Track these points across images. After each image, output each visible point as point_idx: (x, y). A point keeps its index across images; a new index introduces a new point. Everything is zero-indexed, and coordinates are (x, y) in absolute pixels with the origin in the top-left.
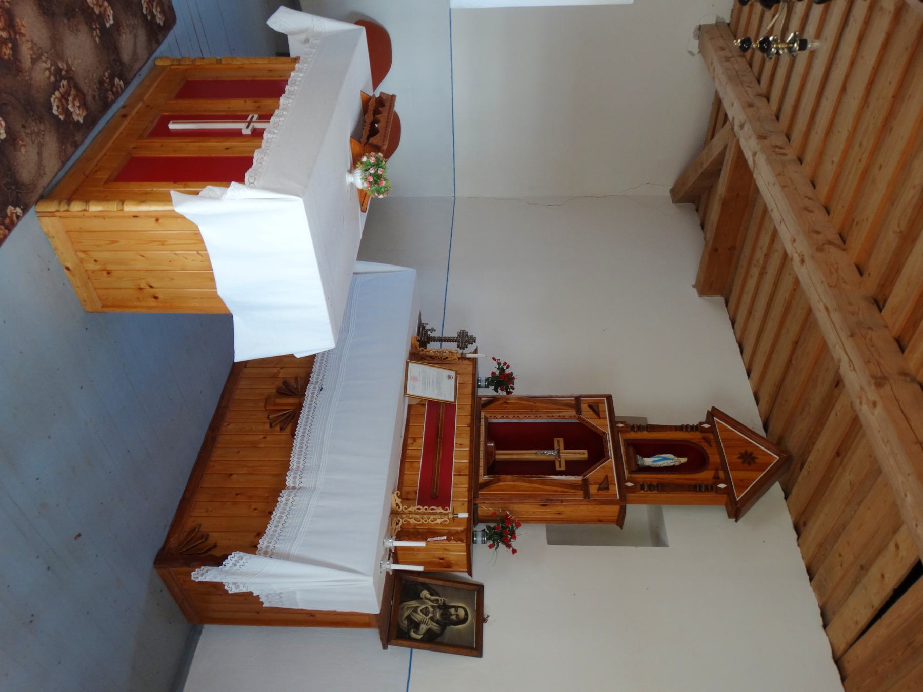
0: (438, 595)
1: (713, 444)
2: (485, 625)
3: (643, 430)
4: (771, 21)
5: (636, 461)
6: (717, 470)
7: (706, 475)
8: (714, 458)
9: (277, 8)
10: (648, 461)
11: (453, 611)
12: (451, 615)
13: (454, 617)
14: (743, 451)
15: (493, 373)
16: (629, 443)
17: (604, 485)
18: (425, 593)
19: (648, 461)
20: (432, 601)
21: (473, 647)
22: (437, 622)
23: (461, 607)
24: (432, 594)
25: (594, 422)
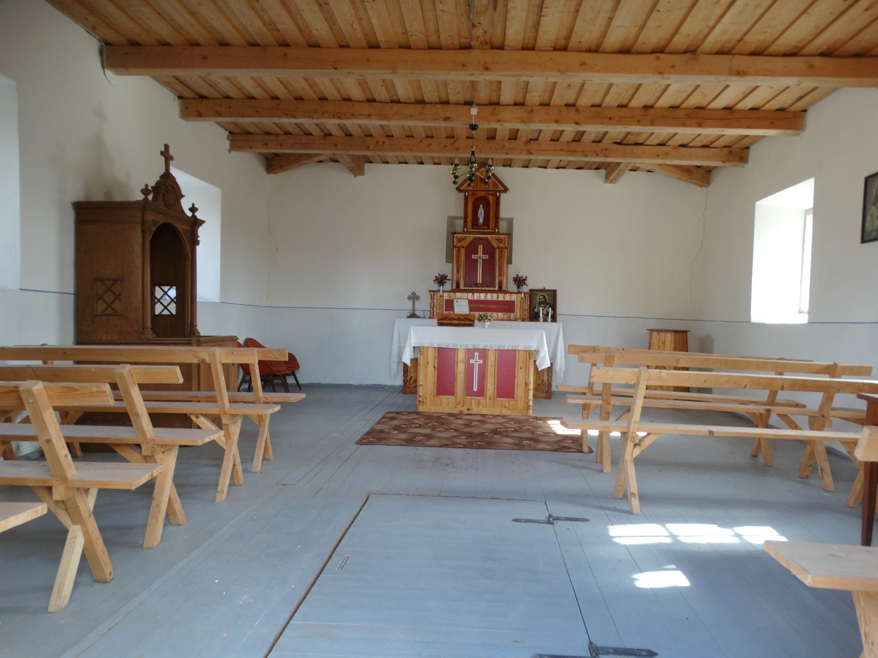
0: (536, 306)
1: (475, 192)
2: (546, 288)
3: (467, 221)
4: (763, 137)
5: (481, 225)
6: (488, 194)
7: (491, 199)
8: (483, 194)
9: (753, 323)
10: (481, 221)
11: (541, 300)
13: (543, 300)
14: (479, 181)
15: (522, 277)
18: (536, 310)
19: (481, 221)
21: (554, 292)
22: (546, 306)
23: (539, 297)
25: (468, 241)
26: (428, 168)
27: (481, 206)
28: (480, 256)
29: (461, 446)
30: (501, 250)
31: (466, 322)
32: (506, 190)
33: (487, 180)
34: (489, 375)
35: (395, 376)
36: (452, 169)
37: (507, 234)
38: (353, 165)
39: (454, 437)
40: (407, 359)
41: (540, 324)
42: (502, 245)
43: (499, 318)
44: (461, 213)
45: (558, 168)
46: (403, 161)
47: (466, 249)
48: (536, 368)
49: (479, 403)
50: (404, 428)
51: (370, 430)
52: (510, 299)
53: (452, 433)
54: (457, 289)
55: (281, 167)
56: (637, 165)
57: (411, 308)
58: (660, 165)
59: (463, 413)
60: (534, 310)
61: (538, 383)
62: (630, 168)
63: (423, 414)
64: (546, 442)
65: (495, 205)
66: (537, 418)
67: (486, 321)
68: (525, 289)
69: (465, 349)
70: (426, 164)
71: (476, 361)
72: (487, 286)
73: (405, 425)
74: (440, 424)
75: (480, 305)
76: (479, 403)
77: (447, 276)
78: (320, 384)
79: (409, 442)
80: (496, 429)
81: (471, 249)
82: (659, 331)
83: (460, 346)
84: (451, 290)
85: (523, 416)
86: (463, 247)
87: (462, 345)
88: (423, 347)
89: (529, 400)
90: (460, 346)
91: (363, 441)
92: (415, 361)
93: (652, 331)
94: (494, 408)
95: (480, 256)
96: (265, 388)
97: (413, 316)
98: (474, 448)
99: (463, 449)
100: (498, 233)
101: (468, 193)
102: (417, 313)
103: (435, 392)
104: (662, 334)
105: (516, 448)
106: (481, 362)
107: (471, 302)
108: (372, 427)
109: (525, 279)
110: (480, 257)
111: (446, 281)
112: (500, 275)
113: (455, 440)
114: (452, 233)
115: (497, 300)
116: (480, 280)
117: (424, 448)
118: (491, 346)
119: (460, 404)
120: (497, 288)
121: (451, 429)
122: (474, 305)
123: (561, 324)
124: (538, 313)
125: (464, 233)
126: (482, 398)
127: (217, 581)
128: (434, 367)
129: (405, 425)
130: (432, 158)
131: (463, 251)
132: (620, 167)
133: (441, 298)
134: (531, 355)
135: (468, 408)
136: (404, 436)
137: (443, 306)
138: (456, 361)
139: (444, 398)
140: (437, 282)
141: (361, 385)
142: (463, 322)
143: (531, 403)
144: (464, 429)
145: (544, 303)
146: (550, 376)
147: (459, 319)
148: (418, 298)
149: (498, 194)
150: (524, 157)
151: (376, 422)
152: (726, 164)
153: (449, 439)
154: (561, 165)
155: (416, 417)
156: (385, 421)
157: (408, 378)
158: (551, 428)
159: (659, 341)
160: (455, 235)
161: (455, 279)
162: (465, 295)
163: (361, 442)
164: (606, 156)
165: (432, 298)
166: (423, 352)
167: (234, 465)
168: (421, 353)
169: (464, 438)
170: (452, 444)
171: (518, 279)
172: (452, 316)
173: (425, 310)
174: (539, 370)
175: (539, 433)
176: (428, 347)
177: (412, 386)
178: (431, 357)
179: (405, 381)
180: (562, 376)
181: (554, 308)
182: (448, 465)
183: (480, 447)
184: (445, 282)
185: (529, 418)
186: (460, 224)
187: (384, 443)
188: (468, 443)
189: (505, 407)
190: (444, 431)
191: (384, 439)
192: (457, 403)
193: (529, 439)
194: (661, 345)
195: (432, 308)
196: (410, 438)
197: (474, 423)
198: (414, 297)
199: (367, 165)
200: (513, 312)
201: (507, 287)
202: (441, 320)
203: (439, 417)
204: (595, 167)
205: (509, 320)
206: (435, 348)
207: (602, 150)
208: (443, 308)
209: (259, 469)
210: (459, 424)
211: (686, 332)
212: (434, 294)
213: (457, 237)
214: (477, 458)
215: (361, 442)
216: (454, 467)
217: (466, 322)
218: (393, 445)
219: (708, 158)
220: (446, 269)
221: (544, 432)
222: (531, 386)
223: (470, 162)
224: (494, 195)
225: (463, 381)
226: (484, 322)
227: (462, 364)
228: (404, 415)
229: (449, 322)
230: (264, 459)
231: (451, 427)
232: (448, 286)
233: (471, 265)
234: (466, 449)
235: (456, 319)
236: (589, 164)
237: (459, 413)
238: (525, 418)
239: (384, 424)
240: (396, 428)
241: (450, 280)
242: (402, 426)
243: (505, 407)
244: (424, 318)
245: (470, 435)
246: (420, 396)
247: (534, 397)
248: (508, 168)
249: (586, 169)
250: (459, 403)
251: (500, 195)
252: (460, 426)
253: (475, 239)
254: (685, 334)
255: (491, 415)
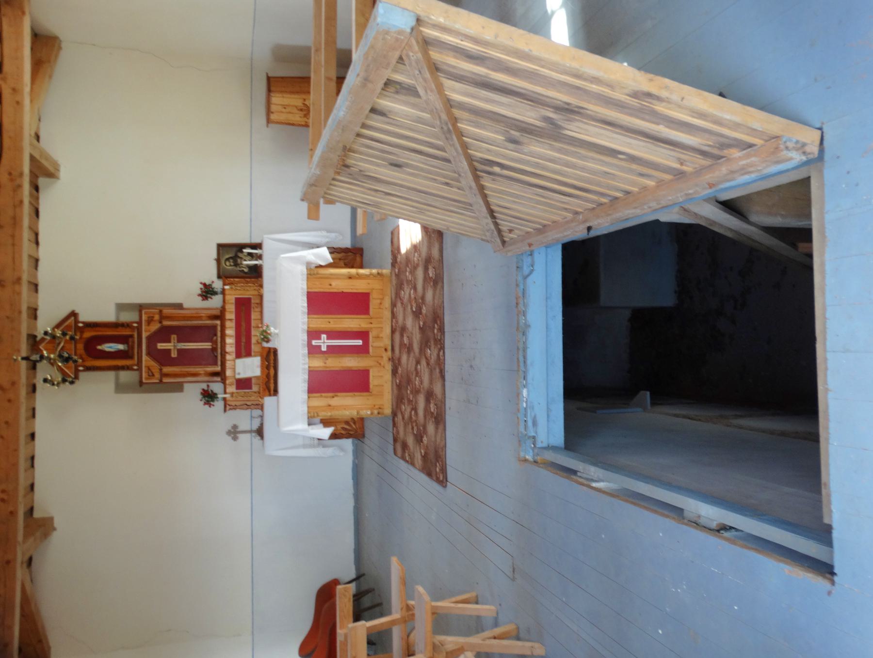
0: (239, 270)
5: (128, 347)
7: (88, 334)
8: (80, 346)
10: (121, 347)
12: (233, 262)
13: (231, 261)
15: (201, 289)
16: (131, 357)
17: (150, 321)
18: (246, 270)
19: (121, 347)
20: (243, 267)
21: (221, 247)
23: (228, 266)
24: (243, 270)
25: (152, 363)
26: (41, 425)
27: (99, 347)
28: (172, 346)
29: (441, 353)
30: (163, 318)
31: (272, 357)
32: (74, 314)
33: (68, 337)
34: (341, 326)
35: (342, 449)
36: (52, 387)
37: (140, 311)
38: (38, 534)
39: (428, 364)
40: (325, 432)
41: (266, 264)
42: (157, 317)
43: (259, 317)
44: (111, 374)
45: (37, 243)
46: (29, 462)
47: (162, 366)
48: (329, 266)
49: (377, 337)
50: (418, 429)
51: (423, 473)
52: (232, 303)
53: (423, 366)
54: (221, 375)
55: (40, 641)
56: (33, 134)
57: (248, 435)
58: (31, 101)
59: (391, 358)
60: (246, 273)
61: (343, 265)
62: (35, 142)
63: (394, 407)
64: (430, 248)
65: (97, 329)
66: (393, 265)
67: (269, 332)
68: (218, 285)
69: (309, 357)
70: (34, 428)
71: (324, 342)
72: (216, 335)
73: (413, 428)
74: (408, 384)
75: (243, 344)
76: (377, 337)
77: (203, 390)
78: (355, 549)
79: (439, 419)
80: (413, 311)
81: (163, 358)
82: (269, 112)
83: (304, 364)
84: (223, 383)
85: (391, 281)
86: (161, 370)
87: (303, 362)
88: (309, 412)
89: (371, 274)
90: (304, 364)
91: (441, 478)
92: (326, 423)
93: (269, 121)
94: (382, 318)
95: (172, 346)
96: (389, 613)
97: (260, 432)
98: (444, 337)
99: (446, 351)
100: (140, 323)
101: (80, 366)
102: (255, 426)
103: (365, 394)
104: (273, 108)
105: (440, 284)
106: (324, 336)
107: (239, 355)
108: (419, 470)
109: (205, 285)
110: (175, 346)
111: (209, 390)
112: (199, 318)
113: (432, 361)
114: (141, 386)
115: (234, 321)
116: (207, 345)
117: (447, 400)
118: (303, 323)
119: (379, 362)
120: (218, 322)
121: (416, 369)
122: (244, 350)
123: (265, 236)
124: (250, 267)
125: (140, 370)
126: (370, 333)
127: (660, 632)
128: (333, 397)
129: (413, 428)
130: (27, 419)
131: (167, 370)
132: (37, 156)
133: (234, 395)
134: (314, 272)
135: (384, 350)
136: (431, 428)
137: (244, 392)
138: (325, 369)
139: (373, 382)
140: (212, 403)
141: (354, 495)
142: (272, 362)
143: (374, 271)
144: (414, 353)
145: (235, 259)
146: (334, 250)
147: (268, 367)
148: (235, 427)
149: (81, 325)
150: (25, 289)
151: (411, 467)
152: (27, 10)
153: (431, 370)
154: (33, 238)
155: (400, 416)
156: (409, 455)
157: (343, 432)
158: (419, 242)
159: (282, 112)
160: (144, 381)
161: (206, 379)
162: (228, 364)
163: (442, 481)
164: (21, 175)
165: (235, 408)
166: (314, 413)
167: (495, 638)
168: (316, 414)
169: (429, 351)
170: (439, 365)
171: (204, 294)
172: (265, 377)
173: (251, 417)
174: (332, 261)
175: (415, 259)
176: (308, 407)
177: (354, 426)
178: (320, 401)
179: (348, 436)
180: (333, 235)
181: (240, 247)
182: (471, 366)
183: (442, 330)
184: (212, 391)
185: (393, 273)
186: (126, 376)
187: (442, 451)
188: (436, 344)
189: (381, 304)
190: (420, 377)
191: (436, 452)
192: (379, 366)
193: (426, 269)
194: (287, 110)
195: (248, 407)
196: (434, 420)
197: (406, 340)
198: (234, 433)
199: (37, 514)
200: (249, 299)
201: (217, 309)
202: (269, 391)
203: (399, 387)
204: (35, 192)
205: (261, 304)
206: (309, 397)
207: (12, 180)
208: (248, 392)
209: (493, 607)
210: (408, 360)
211: (269, 79)
212: (229, 405)
213: (146, 379)
214: (458, 331)
215: (442, 481)
216: (474, 359)
217: (271, 359)
218: (445, 439)
219: (19, 35)
220: (193, 391)
221: (415, 252)
222: (353, 271)
223: (33, 366)
224: (81, 330)
225: (350, 358)
226: (269, 334)
227: (327, 361)
228: (398, 432)
229: (272, 381)
230: (477, 603)
231: (413, 369)
232: (216, 387)
233: (186, 358)
234: (446, 346)
235: (267, 371)
236: (33, 202)
237: (391, 362)
238: (394, 277)
239: (414, 456)
240: (419, 439)
241: (208, 386)
242: (415, 432)
243: (381, 304)
244: (262, 417)
245: (425, 344)
246: (372, 414)
247: (361, 267)
248: (39, 313)
249: (38, 203)
250: (378, 362)
251: (83, 323)
252: (411, 359)
253: (149, 354)
254: (271, 79)
255: (392, 321)
